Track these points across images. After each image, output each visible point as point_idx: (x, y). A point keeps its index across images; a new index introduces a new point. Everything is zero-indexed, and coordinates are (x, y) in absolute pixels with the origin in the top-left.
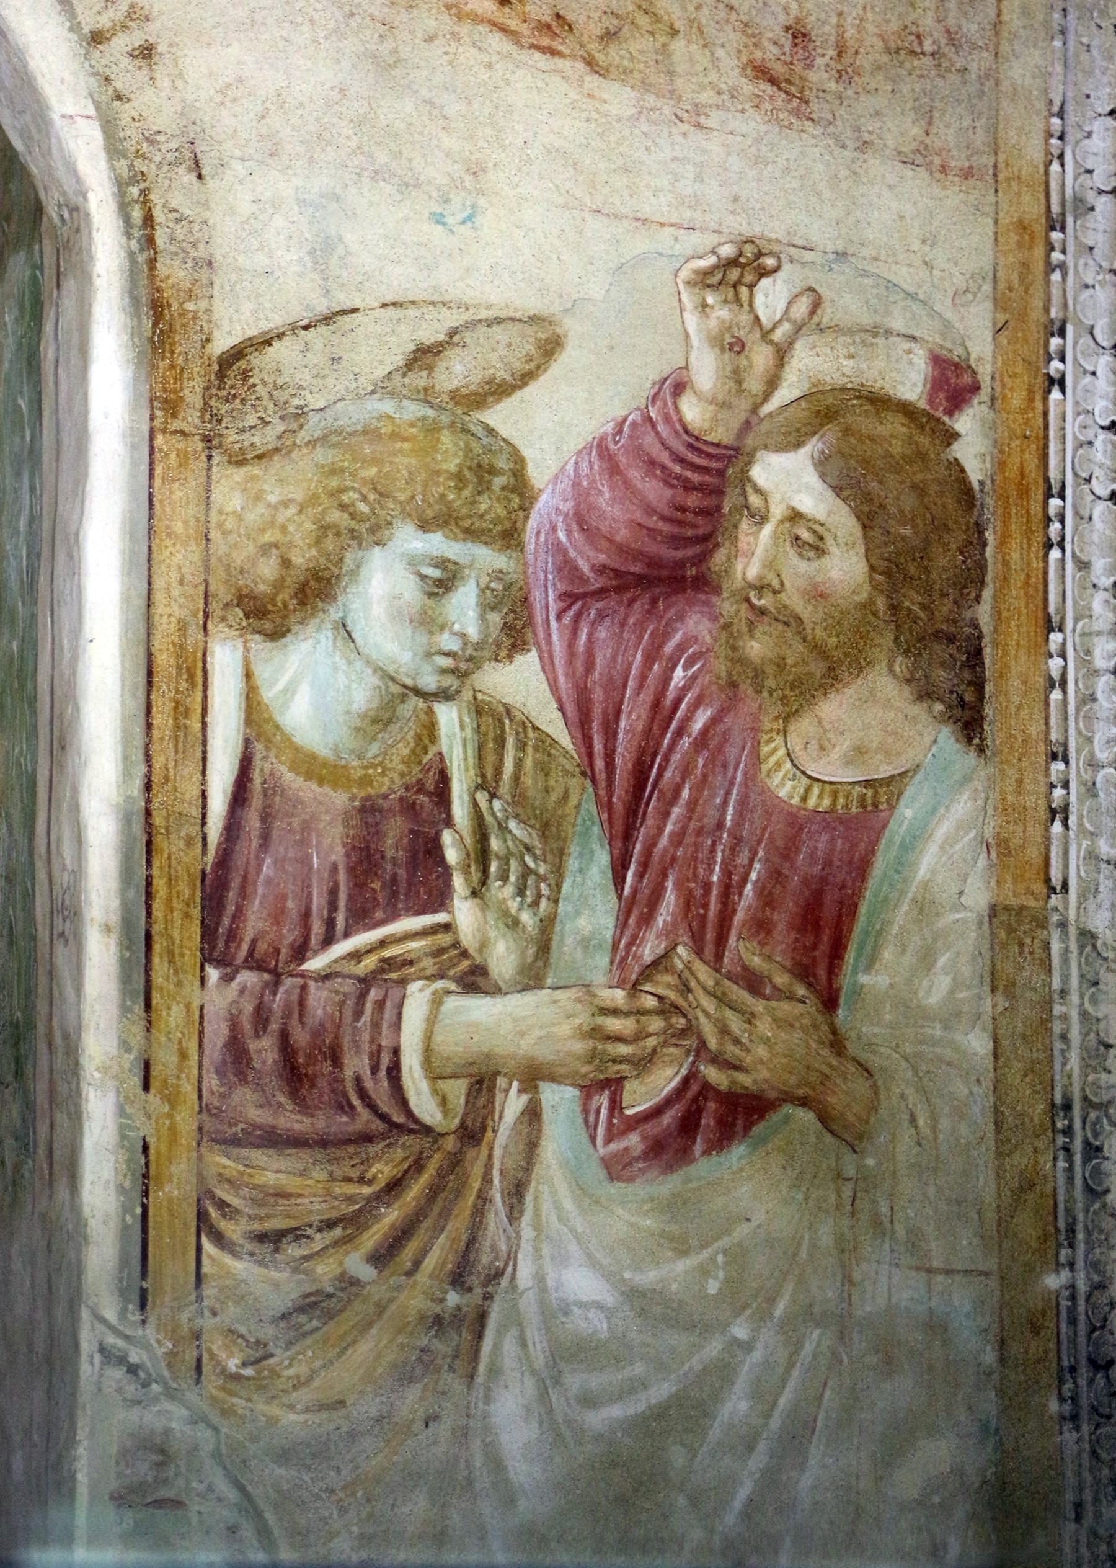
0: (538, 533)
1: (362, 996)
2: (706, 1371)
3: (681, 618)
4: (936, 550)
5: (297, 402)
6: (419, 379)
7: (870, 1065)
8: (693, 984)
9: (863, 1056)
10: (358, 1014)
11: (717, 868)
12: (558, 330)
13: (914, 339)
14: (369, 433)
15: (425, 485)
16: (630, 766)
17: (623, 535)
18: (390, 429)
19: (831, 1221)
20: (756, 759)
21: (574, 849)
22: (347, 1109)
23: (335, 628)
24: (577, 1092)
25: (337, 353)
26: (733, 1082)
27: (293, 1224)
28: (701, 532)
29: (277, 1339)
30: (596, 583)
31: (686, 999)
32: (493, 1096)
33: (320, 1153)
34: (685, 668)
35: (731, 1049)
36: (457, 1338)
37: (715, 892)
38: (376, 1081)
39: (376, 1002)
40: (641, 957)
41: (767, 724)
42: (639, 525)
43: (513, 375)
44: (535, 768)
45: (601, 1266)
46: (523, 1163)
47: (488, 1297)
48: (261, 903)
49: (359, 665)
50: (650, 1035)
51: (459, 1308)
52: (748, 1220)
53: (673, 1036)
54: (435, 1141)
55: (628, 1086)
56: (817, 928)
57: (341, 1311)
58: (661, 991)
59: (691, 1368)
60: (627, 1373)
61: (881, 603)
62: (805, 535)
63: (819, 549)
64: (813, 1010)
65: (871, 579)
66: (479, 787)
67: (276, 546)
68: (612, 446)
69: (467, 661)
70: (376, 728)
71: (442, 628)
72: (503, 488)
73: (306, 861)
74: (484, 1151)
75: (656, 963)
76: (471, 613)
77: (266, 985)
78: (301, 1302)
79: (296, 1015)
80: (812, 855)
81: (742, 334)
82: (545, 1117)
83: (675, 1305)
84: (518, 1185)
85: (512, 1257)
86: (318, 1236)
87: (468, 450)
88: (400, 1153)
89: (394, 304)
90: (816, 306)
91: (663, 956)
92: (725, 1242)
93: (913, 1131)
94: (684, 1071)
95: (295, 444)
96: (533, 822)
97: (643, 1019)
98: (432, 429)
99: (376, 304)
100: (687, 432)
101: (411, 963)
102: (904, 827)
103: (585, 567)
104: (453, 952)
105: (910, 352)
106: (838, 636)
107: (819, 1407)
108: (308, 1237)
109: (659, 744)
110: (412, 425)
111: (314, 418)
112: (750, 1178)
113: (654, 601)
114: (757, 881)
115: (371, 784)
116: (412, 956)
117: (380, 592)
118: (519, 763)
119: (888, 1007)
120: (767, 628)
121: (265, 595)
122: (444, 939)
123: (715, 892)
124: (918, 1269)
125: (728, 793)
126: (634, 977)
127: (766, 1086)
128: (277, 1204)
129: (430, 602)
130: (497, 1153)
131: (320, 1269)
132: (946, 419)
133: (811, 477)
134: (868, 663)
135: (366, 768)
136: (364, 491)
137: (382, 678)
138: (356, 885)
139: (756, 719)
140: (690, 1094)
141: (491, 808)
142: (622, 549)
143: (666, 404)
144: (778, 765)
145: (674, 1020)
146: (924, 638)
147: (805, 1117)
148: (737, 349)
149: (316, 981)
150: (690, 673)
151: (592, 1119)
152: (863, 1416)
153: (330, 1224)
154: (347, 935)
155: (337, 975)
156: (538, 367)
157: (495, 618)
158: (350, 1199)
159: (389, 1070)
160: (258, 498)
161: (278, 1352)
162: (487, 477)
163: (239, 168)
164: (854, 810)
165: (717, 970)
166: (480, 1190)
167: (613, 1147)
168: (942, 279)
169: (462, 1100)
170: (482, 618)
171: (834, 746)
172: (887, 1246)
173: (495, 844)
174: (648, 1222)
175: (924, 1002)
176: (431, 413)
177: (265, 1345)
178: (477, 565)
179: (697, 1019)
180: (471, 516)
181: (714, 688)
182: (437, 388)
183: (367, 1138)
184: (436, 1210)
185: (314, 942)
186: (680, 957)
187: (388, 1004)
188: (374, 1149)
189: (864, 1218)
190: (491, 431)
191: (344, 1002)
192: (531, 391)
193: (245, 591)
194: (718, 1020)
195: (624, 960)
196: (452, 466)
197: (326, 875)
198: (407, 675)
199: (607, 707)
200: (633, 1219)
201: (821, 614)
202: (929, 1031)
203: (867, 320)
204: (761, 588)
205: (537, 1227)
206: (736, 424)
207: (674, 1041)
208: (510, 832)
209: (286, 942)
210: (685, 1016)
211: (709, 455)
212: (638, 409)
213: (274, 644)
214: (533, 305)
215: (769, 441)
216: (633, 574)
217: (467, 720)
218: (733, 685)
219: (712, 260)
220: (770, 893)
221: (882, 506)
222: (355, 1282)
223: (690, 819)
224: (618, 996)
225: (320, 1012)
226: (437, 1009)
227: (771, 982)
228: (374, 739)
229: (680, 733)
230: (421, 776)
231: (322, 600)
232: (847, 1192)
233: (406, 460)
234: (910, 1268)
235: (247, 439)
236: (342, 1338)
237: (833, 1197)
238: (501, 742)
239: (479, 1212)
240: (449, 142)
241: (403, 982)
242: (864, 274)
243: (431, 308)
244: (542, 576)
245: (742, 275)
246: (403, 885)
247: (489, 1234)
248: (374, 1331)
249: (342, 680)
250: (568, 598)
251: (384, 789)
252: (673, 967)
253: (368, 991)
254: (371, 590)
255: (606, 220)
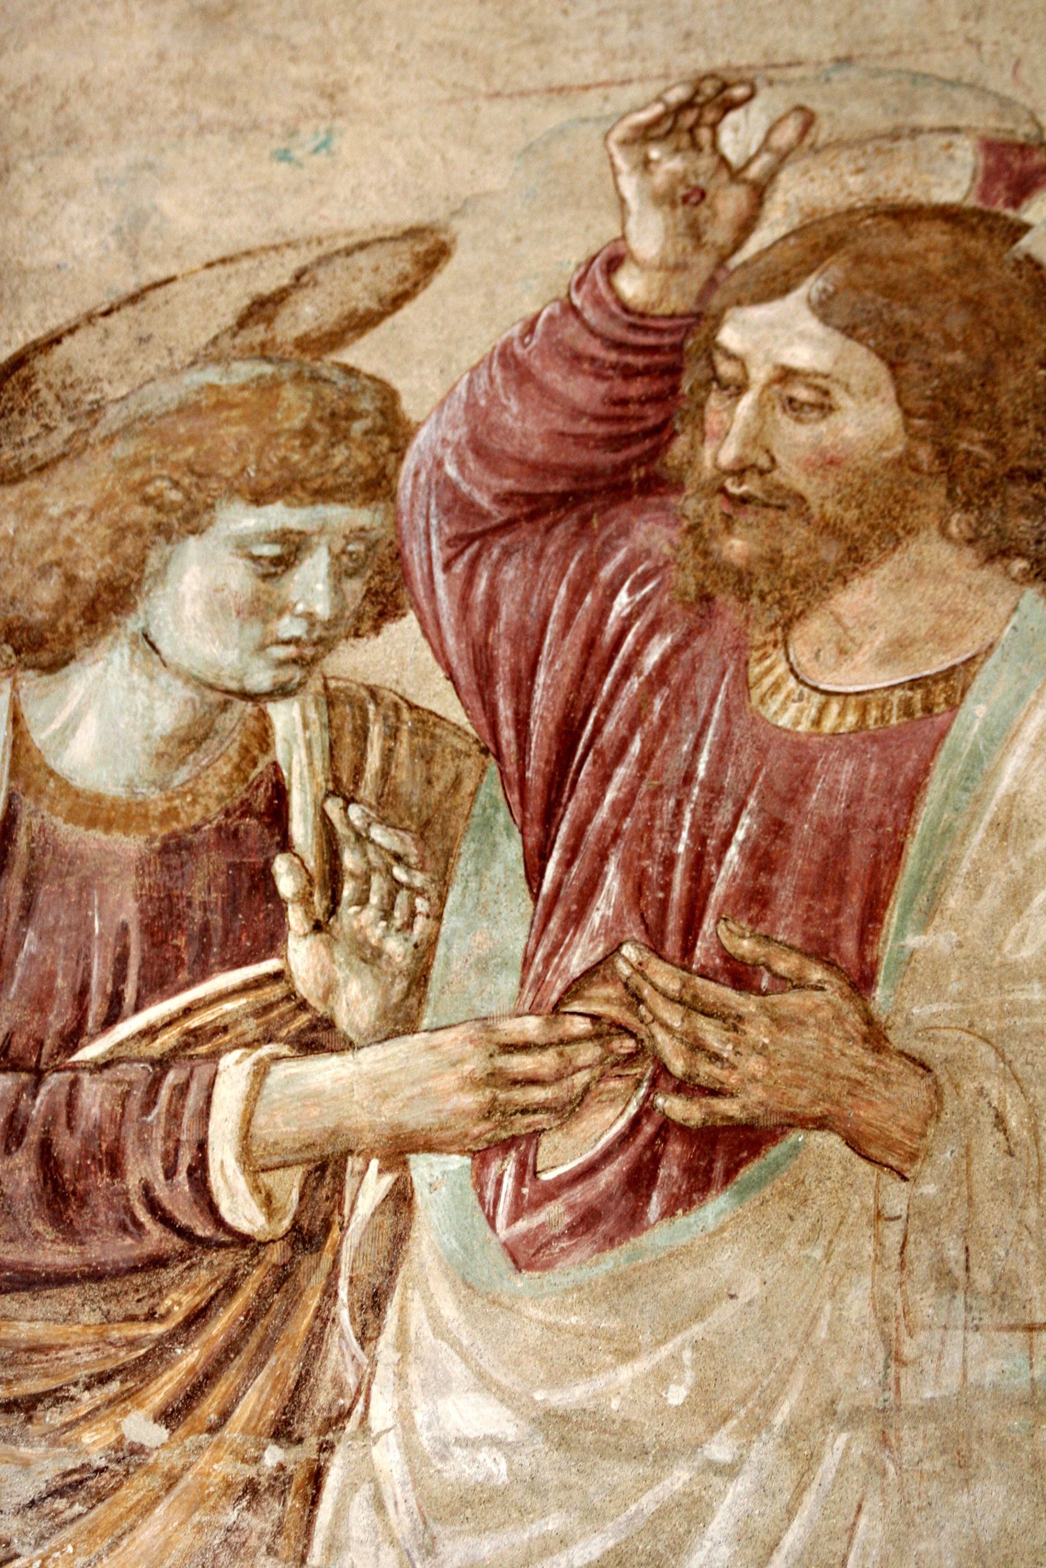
0: (417, 474)
1: (155, 1084)
2: (663, 1512)
3: (625, 532)
4: (1005, 370)
5: (91, 397)
6: (257, 334)
7: (926, 1058)
8: (647, 992)
9: (916, 1046)
10: (149, 1104)
11: (685, 834)
12: (443, 237)
13: (956, 130)
14: (186, 410)
15: (261, 452)
16: (552, 728)
17: (538, 450)
18: (213, 399)
19: (867, 1281)
20: (743, 684)
21: (467, 848)
22: (131, 1228)
23: (134, 642)
24: (467, 1161)
25: (145, 331)
26: (712, 1114)
27: (52, 1384)
28: (650, 423)
29: (25, 1534)
30: (499, 515)
31: (636, 1013)
32: (342, 1182)
33: (94, 1290)
34: (631, 592)
35: (706, 1070)
36: (278, 1507)
37: (680, 867)
38: (172, 1188)
39: (175, 1088)
40: (566, 969)
41: (758, 636)
42: (562, 434)
43: (380, 300)
44: (412, 754)
45: (499, 1387)
46: (386, 1266)
47: (326, 1448)
48: (20, 987)
49: (164, 678)
50: (579, 1069)
51: (281, 1467)
52: (732, 1297)
53: (614, 1065)
54: (255, 1253)
55: (546, 1142)
56: (842, 888)
57: (115, 1489)
58: (596, 1009)
59: (639, 1512)
60: (535, 1529)
61: (924, 454)
62: (802, 394)
63: (825, 408)
64: (836, 998)
65: (907, 427)
66: (330, 794)
67: (58, 564)
68: (519, 351)
69: (315, 644)
70: (185, 749)
71: (280, 613)
72: (366, 433)
73: (83, 926)
74: (327, 1257)
75: (589, 973)
76: (320, 587)
77: (24, 1087)
78: (59, 1482)
79: (63, 1119)
80: (830, 794)
81: (702, 181)
82: (418, 1199)
83: (616, 1426)
84: (375, 1295)
85: (363, 1391)
86: (86, 1395)
87: (319, 398)
88: (205, 1275)
89: (223, 261)
90: (809, 121)
91: (600, 963)
92: (697, 1330)
93: (1000, 1137)
94: (632, 1110)
95: (87, 443)
96: (407, 823)
97: (568, 1049)
98: (269, 388)
99: (198, 266)
100: (626, 309)
101: (225, 1029)
102: (976, 728)
103: (483, 500)
104: (285, 1007)
105: (950, 146)
106: (860, 506)
107: (850, 1543)
108: (72, 1399)
109: (595, 693)
110: (243, 388)
111: (112, 411)
112: (735, 1240)
113: (585, 521)
114: (744, 841)
115: (177, 818)
116: (227, 1020)
117: (195, 587)
118: (388, 755)
119: (954, 974)
120: (751, 519)
121: (43, 622)
122: (274, 992)
123: (680, 867)
124: (1012, 1328)
125: (701, 734)
126: (554, 997)
127: (759, 1111)
128: (31, 1363)
129: (262, 586)
130: (346, 1257)
131: (87, 1438)
132: (1010, 212)
133: (812, 325)
134: (909, 532)
135: (170, 799)
136: (176, 476)
137: (197, 687)
138: (154, 945)
139: (742, 633)
140: (641, 1140)
141: (347, 816)
142: (538, 468)
143: (595, 285)
144: (776, 686)
145: (616, 1044)
146: (992, 483)
147: (829, 1143)
148: (694, 199)
149: (92, 1072)
150: (638, 597)
151: (489, 1194)
152: (922, 1546)
153: (103, 1379)
154: (137, 1009)
155: (120, 1060)
156: (416, 285)
157: (355, 587)
158: (132, 1343)
159: (191, 1171)
160: (37, 514)
161: (25, 1550)
162: (343, 424)
163: (28, 167)
164: (894, 721)
165: (685, 968)
166: (319, 1308)
167: (522, 1225)
168: (995, 54)
169: (295, 1195)
170: (337, 589)
171: (860, 646)
172: (959, 1302)
173: (350, 860)
174: (574, 1320)
175: (1013, 957)
176: (268, 369)
177: (8, 1544)
178: (329, 528)
179: (652, 1037)
180: (322, 475)
181: (677, 608)
182: (279, 339)
183: (157, 1262)
184: (254, 1341)
185: (90, 1024)
186: (626, 960)
187: (194, 1086)
188: (167, 1275)
189: (921, 1269)
190: (349, 371)
191: (128, 1094)
192: (408, 311)
193: (15, 624)
194: (686, 1034)
195: (540, 979)
196: (297, 422)
197: (111, 940)
198: (232, 678)
199: (517, 663)
200: (551, 1319)
201: (832, 485)
202: (1021, 997)
203: (884, 123)
204: (740, 472)
205: (402, 1344)
206: (695, 286)
207: (617, 1071)
208: (373, 842)
209: (52, 1032)
210: (633, 1035)
211: (659, 331)
212: (556, 300)
213: (51, 677)
214: (410, 216)
215: (743, 295)
216: (554, 494)
217: (313, 715)
218: (706, 598)
219: (658, 109)
220: (767, 853)
221: (918, 336)
222: (137, 1450)
223: (642, 778)
224: (531, 1027)
225: (95, 1111)
226: (261, 1084)
227: (769, 969)
228: (183, 761)
229: (626, 673)
230: (246, 796)
231: (116, 613)
232: (892, 1235)
233: (234, 430)
234: (999, 1329)
235: (25, 453)
236: (115, 1524)
237: (869, 1248)
238: (362, 734)
239: (316, 1339)
240: (302, 71)
241: (214, 1056)
242: (879, 73)
243: (272, 253)
244: (421, 523)
245: (700, 116)
246: (217, 938)
247: (330, 1364)
248: (159, 1511)
249: (141, 698)
250: (459, 543)
251: (196, 820)
252: (615, 973)
253: (165, 1073)
254: (183, 589)
255: (506, 103)
